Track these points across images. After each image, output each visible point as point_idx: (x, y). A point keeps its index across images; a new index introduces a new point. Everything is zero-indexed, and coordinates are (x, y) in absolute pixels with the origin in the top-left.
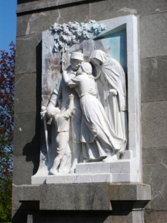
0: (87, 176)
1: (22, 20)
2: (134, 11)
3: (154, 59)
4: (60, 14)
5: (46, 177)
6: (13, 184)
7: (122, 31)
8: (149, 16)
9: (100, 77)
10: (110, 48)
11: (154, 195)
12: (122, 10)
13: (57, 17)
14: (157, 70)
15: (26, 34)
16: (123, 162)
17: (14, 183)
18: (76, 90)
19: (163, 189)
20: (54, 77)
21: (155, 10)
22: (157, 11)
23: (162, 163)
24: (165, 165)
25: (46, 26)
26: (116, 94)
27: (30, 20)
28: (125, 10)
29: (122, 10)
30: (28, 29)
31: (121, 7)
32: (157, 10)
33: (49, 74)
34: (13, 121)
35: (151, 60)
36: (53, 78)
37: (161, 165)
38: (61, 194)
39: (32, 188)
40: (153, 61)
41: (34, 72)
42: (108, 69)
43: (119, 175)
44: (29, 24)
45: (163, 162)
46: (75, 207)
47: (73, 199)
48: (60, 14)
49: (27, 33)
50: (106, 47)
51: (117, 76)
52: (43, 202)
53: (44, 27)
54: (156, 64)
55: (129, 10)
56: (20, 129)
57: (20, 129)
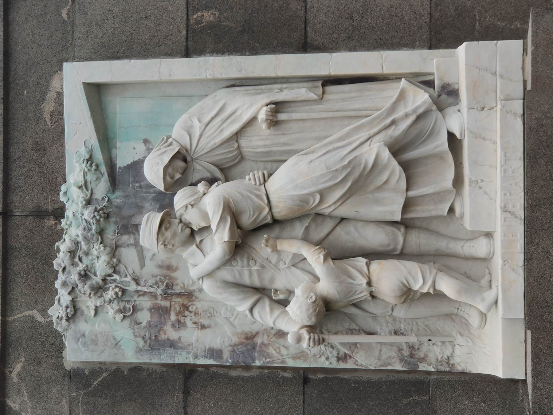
0: (504, 179)
4: (29, 313)
5: (505, 319)
8: (76, 34)
9: (222, 170)
12: (47, 117)
13: (33, 318)
16: (529, 17)
20: (206, 322)
21: (65, 22)
26: (273, 106)
28: (48, 107)
29: (47, 117)
31: (40, 119)
34: (115, 231)
36: (209, 327)
39: (536, 375)
40: (198, 22)
41: (174, 362)
42: (201, 136)
43: (501, 76)
48: (29, 313)
54: (206, 14)
55: (51, 95)
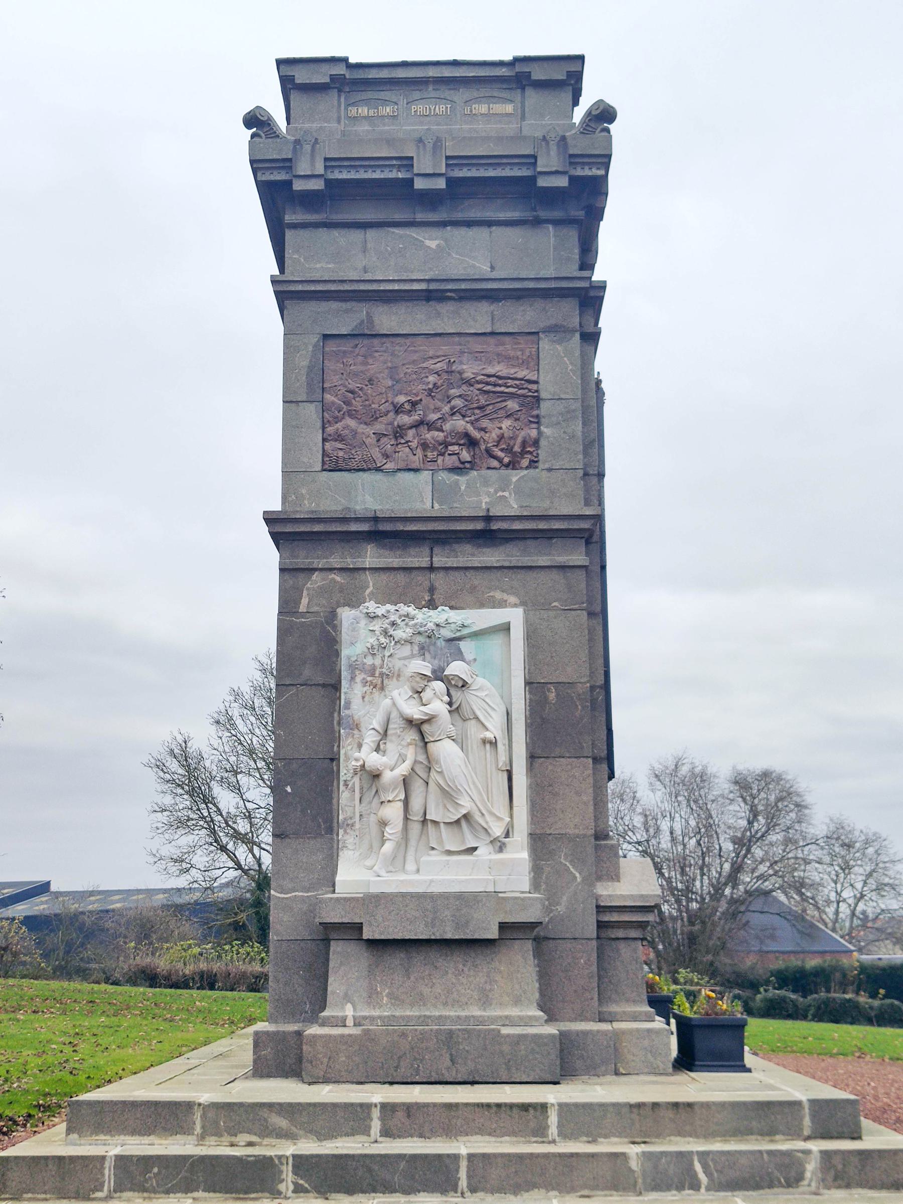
1: (291, 582)
2: (512, 599)
3: (549, 686)
4: (371, 584)
6: (272, 892)
7: (506, 628)
10: (475, 660)
11: (550, 913)
14: (554, 704)
15: (300, 611)
17: (275, 891)
18: (426, 728)
19: (563, 904)
20: (366, 699)
21: (550, 604)
22: (555, 606)
23: (564, 862)
24: (568, 864)
25: (342, 601)
27: (309, 585)
30: (305, 601)
31: (491, 589)
32: (554, 604)
33: (356, 692)
35: (543, 687)
36: (363, 701)
37: (561, 863)
38: (406, 911)
39: (338, 899)
40: (549, 690)
43: (508, 879)
44: (305, 593)
45: (566, 859)
46: (434, 934)
47: (429, 920)
48: (371, 584)
49: (302, 608)
50: (469, 656)
51: (493, 709)
52: (371, 925)
53: (501, 588)
54: (553, 694)
56: (289, 789)
57: (289, 789)
